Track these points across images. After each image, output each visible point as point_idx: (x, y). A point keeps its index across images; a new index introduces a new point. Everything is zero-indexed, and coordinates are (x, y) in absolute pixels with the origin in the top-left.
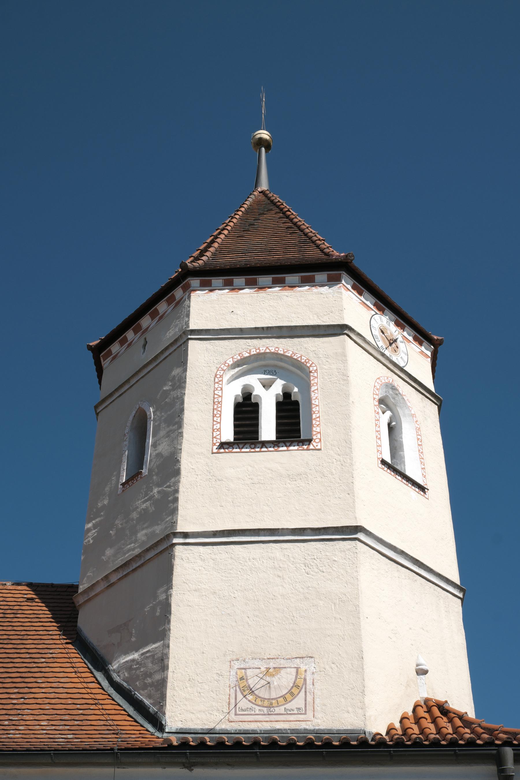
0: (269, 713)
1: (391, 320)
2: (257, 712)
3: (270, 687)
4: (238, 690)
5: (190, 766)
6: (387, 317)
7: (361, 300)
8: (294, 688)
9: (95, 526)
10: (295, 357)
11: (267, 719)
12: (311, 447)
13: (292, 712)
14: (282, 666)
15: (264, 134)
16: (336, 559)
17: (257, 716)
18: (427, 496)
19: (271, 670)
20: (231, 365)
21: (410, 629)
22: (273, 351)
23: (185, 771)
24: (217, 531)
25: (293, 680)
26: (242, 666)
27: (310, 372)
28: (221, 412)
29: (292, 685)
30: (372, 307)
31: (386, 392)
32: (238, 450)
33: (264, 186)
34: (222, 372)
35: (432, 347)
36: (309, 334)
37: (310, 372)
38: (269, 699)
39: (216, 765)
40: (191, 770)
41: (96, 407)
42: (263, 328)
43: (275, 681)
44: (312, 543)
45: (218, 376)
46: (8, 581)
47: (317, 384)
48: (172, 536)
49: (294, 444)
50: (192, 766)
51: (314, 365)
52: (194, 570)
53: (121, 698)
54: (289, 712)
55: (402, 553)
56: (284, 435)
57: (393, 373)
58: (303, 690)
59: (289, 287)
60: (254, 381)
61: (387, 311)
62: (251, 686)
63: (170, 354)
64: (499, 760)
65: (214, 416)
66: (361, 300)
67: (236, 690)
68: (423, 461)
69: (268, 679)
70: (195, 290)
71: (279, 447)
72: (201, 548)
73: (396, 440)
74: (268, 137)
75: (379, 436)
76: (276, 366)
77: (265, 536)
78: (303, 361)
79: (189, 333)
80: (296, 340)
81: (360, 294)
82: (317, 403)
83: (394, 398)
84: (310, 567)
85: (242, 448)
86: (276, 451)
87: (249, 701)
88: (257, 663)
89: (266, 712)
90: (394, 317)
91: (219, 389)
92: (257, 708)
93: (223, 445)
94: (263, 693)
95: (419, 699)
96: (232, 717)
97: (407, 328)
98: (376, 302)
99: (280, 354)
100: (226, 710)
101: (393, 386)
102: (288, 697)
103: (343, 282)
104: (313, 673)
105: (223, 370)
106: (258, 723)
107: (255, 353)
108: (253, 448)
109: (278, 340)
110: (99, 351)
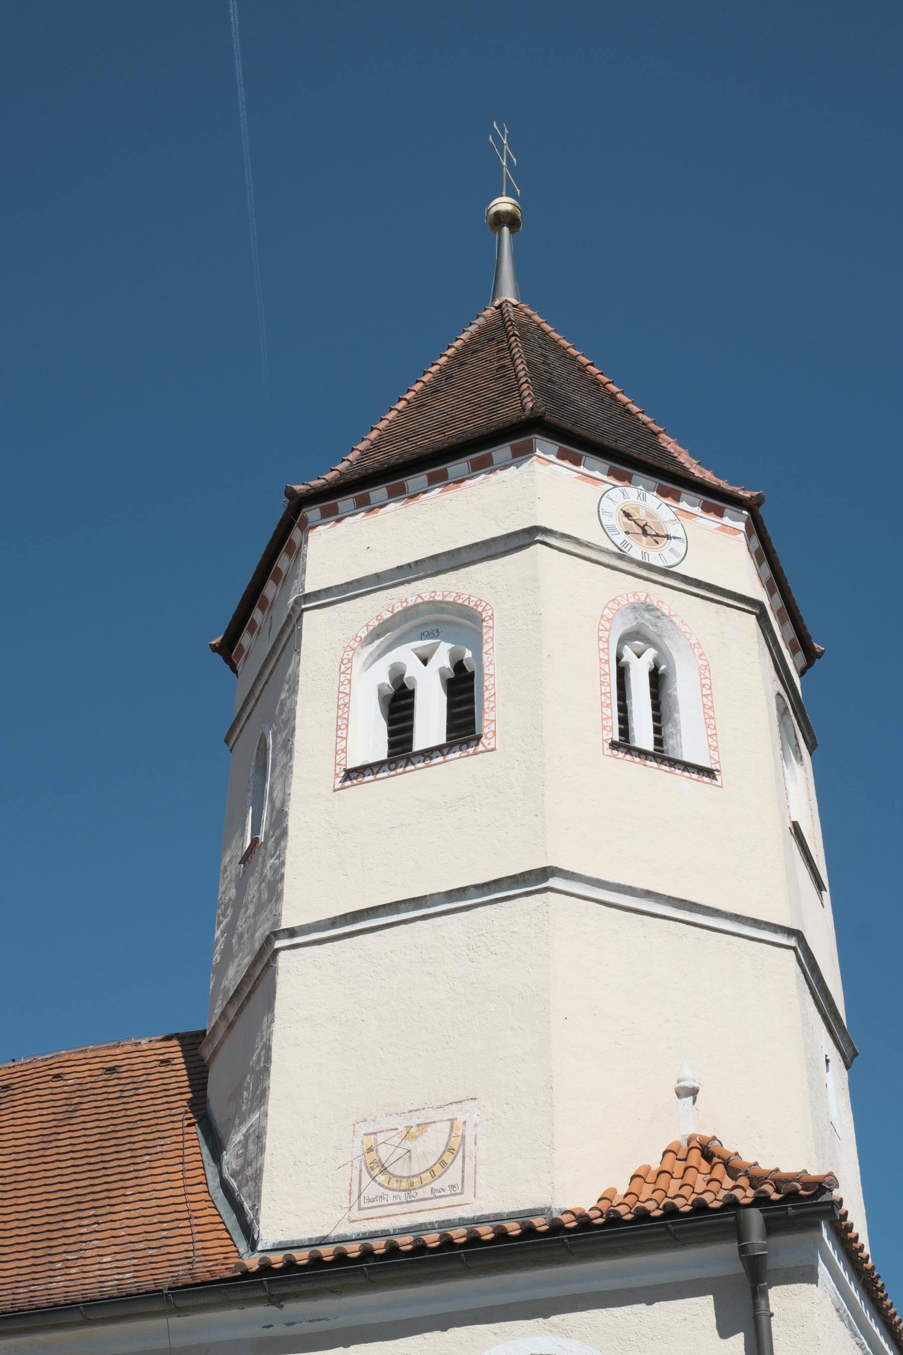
0: (409, 1199)
1: (649, 490)
2: (391, 1201)
3: (410, 1157)
4: (364, 1168)
5: (277, 1300)
6: (641, 487)
7: (579, 473)
8: (447, 1153)
9: (222, 933)
10: (460, 601)
11: (406, 1210)
12: (480, 748)
13: (442, 1193)
14: (429, 1121)
15: (504, 204)
16: (515, 929)
17: (390, 1207)
18: (718, 783)
19: (413, 1130)
20: (366, 638)
21: (668, 1020)
22: (426, 599)
23: (273, 1309)
24: (335, 918)
25: (446, 1141)
26: (371, 1130)
27: (483, 621)
28: (347, 719)
29: (443, 1149)
30: (605, 478)
31: (636, 618)
32: (372, 777)
33: (508, 294)
34: (351, 653)
35: (745, 512)
36: (481, 556)
37: (483, 621)
38: (409, 1177)
39: (315, 1294)
40: (281, 1307)
41: (227, 741)
42: (409, 565)
43: (418, 1147)
44: (480, 909)
45: (345, 661)
46: (143, 1037)
47: (492, 638)
48: (273, 937)
49: (454, 749)
50: (282, 1300)
51: (488, 607)
52: (306, 986)
53: (227, 1202)
54: (437, 1194)
55: (648, 894)
56: (461, 733)
57: (649, 583)
58: (460, 1154)
59: (455, 482)
60: (405, 655)
61: (637, 476)
62: (383, 1161)
63: (288, 639)
64: (738, 1232)
65: (338, 728)
66: (579, 473)
67: (361, 1170)
68: (712, 721)
69: (408, 1144)
70: (315, 527)
71: (431, 759)
72: (316, 949)
73: (670, 696)
74: (509, 207)
75: (710, 704)
76: (438, 622)
77: (407, 911)
78: (472, 605)
79: (302, 600)
80: (463, 571)
81: (577, 462)
82: (491, 672)
83: (655, 625)
84: (476, 949)
85: (377, 773)
86: (428, 766)
87: (380, 1184)
88: (394, 1122)
89: (403, 1200)
90: (653, 482)
91: (347, 682)
92: (391, 1194)
93: (352, 774)
94: (399, 1169)
95: (679, 1139)
96: (355, 1214)
97: (686, 494)
98: (611, 467)
99: (437, 602)
100: (346, 1204)
101: (650, 605)
102: (438, 1169)
103: (538, 452)
104: (476, 1125)
105: (353, 649)
106: (392, 1218)
107: (400, 609)
108: (394, 770)
109: (435, 578)
110: (228, 648)
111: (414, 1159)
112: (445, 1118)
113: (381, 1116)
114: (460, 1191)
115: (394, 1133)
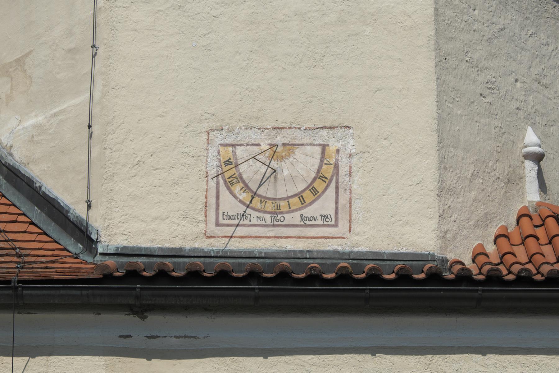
0: (275, 223)
2: (254, 221)
3: (276, 178)
8: (318, 181)
11: (272, 234)
13: (313, 222)
25: (316, 167)
29: (313, 175)
38: (274, 199)
40: (144, 318)
43: (285, 169)
54: (308, 223)
58: (333, 184)
89: (269, 222)
96: (212, 228)
111: (280, 182)
112: (316, 143)
113: (240, 128)
114: (333, 222)
115: (256, 149)
